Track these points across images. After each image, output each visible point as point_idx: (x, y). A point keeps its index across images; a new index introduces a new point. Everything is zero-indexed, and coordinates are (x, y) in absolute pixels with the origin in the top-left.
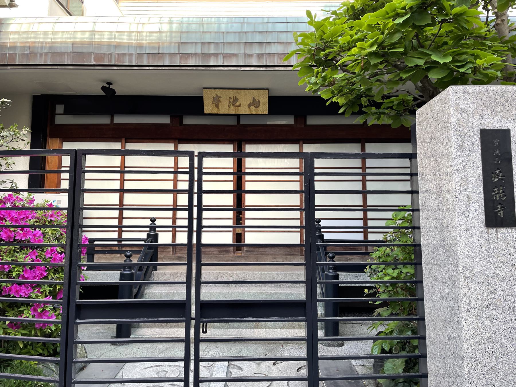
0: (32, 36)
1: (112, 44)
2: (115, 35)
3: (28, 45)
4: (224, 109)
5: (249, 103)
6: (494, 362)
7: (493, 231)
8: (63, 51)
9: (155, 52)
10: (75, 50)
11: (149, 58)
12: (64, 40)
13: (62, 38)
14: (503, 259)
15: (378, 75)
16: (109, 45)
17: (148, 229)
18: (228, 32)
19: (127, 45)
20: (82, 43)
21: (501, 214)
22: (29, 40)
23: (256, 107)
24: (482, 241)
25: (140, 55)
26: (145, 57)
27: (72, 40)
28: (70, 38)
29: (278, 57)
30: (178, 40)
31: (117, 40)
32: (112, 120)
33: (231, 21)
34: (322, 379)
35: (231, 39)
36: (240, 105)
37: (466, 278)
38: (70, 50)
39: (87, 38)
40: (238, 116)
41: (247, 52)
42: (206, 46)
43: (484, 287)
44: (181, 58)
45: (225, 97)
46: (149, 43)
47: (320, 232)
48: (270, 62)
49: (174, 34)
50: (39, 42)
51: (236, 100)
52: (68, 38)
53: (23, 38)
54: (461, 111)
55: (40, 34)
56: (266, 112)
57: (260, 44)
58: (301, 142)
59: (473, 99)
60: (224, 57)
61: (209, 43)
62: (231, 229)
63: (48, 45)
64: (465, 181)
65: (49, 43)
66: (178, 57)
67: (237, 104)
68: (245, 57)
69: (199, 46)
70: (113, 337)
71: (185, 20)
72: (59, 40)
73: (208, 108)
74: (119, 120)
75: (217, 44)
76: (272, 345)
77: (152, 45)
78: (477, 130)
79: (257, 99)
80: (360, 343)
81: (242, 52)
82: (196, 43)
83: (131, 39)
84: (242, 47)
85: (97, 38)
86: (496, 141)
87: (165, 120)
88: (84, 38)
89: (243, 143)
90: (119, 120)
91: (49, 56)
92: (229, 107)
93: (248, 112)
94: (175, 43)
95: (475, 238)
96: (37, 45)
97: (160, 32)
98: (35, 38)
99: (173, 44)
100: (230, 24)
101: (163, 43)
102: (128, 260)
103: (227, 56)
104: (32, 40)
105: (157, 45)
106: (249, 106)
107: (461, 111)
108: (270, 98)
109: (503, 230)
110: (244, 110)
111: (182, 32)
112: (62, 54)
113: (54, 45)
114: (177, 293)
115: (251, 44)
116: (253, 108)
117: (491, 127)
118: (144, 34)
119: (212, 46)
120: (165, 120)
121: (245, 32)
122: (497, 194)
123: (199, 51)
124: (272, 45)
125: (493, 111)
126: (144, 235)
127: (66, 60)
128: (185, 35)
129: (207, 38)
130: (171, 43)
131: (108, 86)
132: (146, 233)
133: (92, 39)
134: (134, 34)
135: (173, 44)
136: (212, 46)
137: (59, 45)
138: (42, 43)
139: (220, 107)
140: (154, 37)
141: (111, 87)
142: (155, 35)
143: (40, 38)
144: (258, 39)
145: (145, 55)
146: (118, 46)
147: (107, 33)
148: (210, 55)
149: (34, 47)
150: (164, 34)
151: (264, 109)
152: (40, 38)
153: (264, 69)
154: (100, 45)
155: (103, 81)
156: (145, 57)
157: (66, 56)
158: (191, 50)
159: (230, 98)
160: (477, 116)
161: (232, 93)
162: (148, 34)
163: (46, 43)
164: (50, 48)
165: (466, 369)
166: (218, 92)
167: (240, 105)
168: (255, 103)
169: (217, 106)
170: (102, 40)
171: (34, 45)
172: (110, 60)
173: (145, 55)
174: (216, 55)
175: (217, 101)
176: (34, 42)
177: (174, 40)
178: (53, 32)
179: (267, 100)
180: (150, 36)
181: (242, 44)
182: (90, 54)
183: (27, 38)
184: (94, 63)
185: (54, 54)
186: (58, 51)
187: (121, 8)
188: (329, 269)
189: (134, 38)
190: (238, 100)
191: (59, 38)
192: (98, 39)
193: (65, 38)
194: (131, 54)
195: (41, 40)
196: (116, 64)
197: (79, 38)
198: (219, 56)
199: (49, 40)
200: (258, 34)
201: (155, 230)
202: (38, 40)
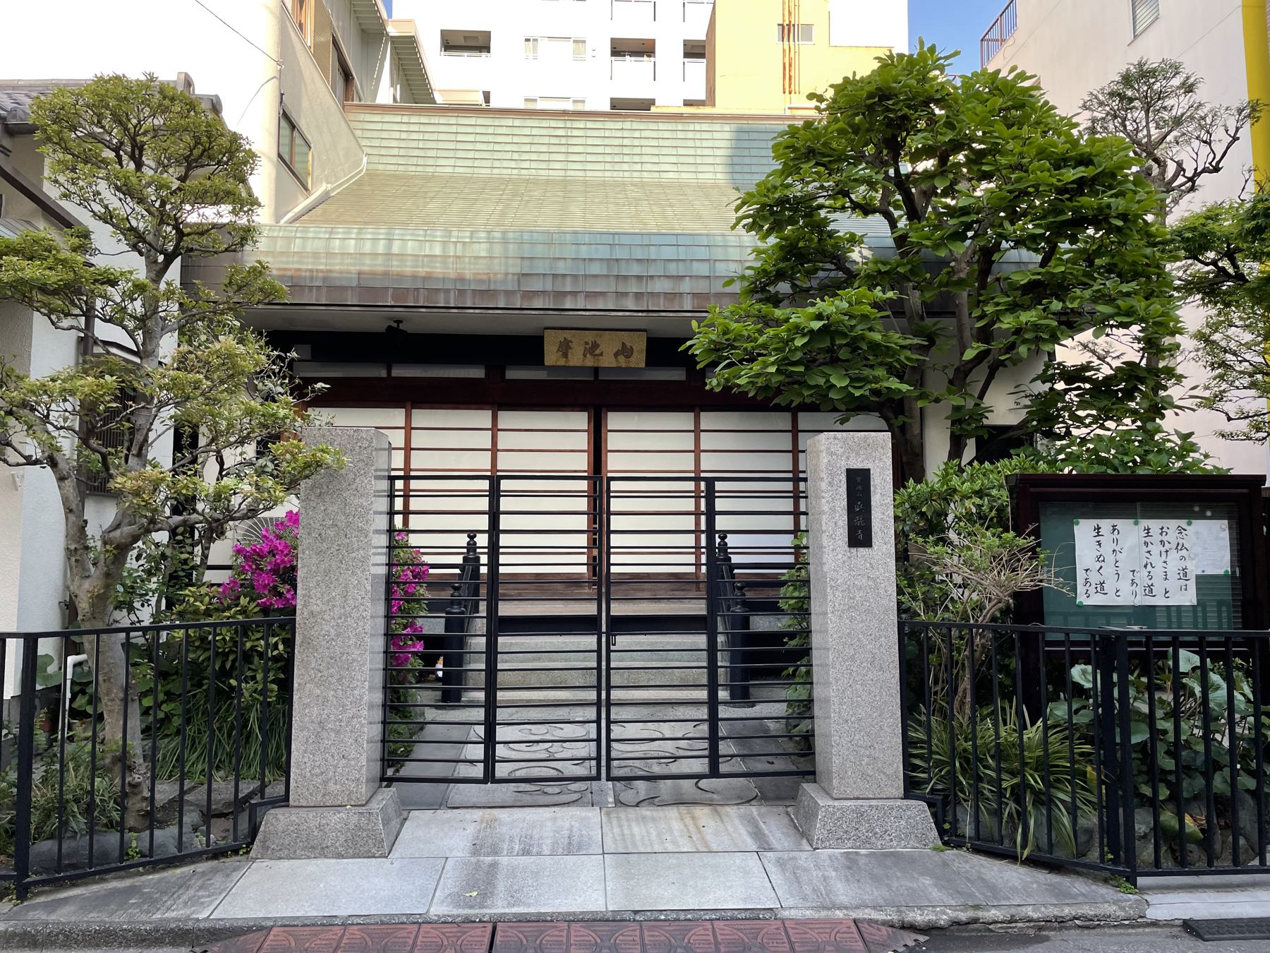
0: (295, 259)
1: (420, 275)
2: (423, 261)
3: (289, 273)
4: (577, 358)
5: (615, 350)
6: (852, 652)
7: (854, 550)
8: (345, 283)
9: (484, 287)
10: (363, 284)
11: (474, 297)
12: (345, 268)
13: (341, 264)
14: (861, 572)
15: (812, 331)
16: (414, 277)
17: (465, 550)
18: (591, 259)
19: (441, 276)
20: (373, 274)
21: (861, 537)
22: (291, 266)
23: (627, 357)
24: (845, 558)
25: (461, 292)
26: (469, 294)
27: (358, 268)
28: (355, 265)
29: (665, 297)
30: (517, 270)
31: (425, 269)
32: (389, 372)
33: (597, 238)
34: (723, 738)
35: (596, 269)
36: (601, 354)
37: (832, 587)
38: (354, 284)
39: (380, 265)
40: (596, 370)
41: (619, 290)
42: (560, 279)
43: (846, 594)
44: (522, 297)
45: (578, 343)
46: (474, 274)
47: (726, 553)
48: (653, 306)
49: (511, 261)
50: (306, 270)
51: (595, 345)
52: (351, 264)
53: (281, 262)
54: (832, 454)
55: (308, 257)
56: (643, 365)
57: (639, 278)
58: (697, 410)
59: (841, 444)
60: (586, 296)
61: (564, 276)
62: (585, 550)
63: (321, 275)
64: (833, 510)
65: (322, 271)
66: (519, 296)
67: (598, 352)
68: (617, 296)
69: (549, 280)
70: (439, 701)
71: (526, 237)
72: (337, 268)
73: (552, 356)
74: (399, 372)
75: (575, 277)
76: (658, 708)
77: (479, 277)
78: (844, 469)
79: (628, 345)
80: (778, 705)
81: (613, 289)
82: (544, 275)
83: (448, 268)
84: (613, 281)
85: (395, 267)
86: (859, 479)
87: (477, 373)
88: (375, 265)
89: (604, 410)
90: (399, 372)
91: (324, 291)
92: (585, 356)
93: (614, 365)
94: (514, 274)
95: (840, 556)
96: (304, 274)
97: (490, 257)
98: (299, 262)
99: (510, 276)
100: (593, 247)
101: (495, 274)
102: (456, 594)
103: (590, 295)
104: (296, 266)
105: (485, 277)
106: (616, 355)
107: (832, 454)
108: (649, 340)
109: (861, 549)
110: (608, 361)
111: (522, 258)
112: (343, 289)
113: (330, 274)
114: (517, 644)
115: (626, 277)
116: (621, 358)
117: (855, 467)
118: (467, 260)
119: (569, 280)
120: (477, 373)
121: (617, 260)
122: (859, 521)
123: (549, 287)
124: (656, 279)
125: (857, 454)
126: (459, 560)
127: (349, 298)
128: (526, 263)
129: (562, 268)
130: (507, 274)
131: (395, 325)
132: (461, 557)
133: (388, 266)
134: (451, 259)
135: (510, 276)
136: (569, 280)
137: (338, 275)
138: (311, 271)
139: (570, 356)
140: (481, 268)
141: (402, 327)
142: (481, 261)
143: (307, 263)
144: (636, 270)
145: (469, 292)
146: (427, 278)
147: (410, 258)
148: (565, 294)
149: (300, 277)
150: (496, 261)
151: (639, 360)
152: (307, 263)
153: (644, 314)
154: (401, 276)
155: (391, 319)
156: (469, 294)
157: (349, 292)
158: (537, 285)
159: (587, 343)
160: (844, 458)
161: (590, 337)
162: (472, 260)
163: (317, 271)
164: (325, 279)
165: (831, 657)
166: (568, 335)
167: (601, 354)
168: (626, 351)
169: (565, 355)
170: (404, 269)
171: (298, 273)
172: (416, 300)
173: (469, 292)
174: (574, 294)
175: (565, 348)
176: (299, 270)
177: (511, 270)
178: (327, 253)
179: (644, 346)
180: (475, 264)
181: (612, 278)
182: (387, 288)
183: (288, 263)
184: (393, 304)
185: (332, 289)
186: (338, 284)
187: (353, 125)
188: (737, 604)
189: (451, 266)
190: (598, 346)
191: (337, 266)
192: (398, 266)
193: (348, 264)
194: (447, 291)
195: (310, 267)
196: (426, 305)
197: (367, 265)
198: (579, 295)
199: (322, 267)
200: (635, 263)
201: (475, 551)
202: (304, 267)
